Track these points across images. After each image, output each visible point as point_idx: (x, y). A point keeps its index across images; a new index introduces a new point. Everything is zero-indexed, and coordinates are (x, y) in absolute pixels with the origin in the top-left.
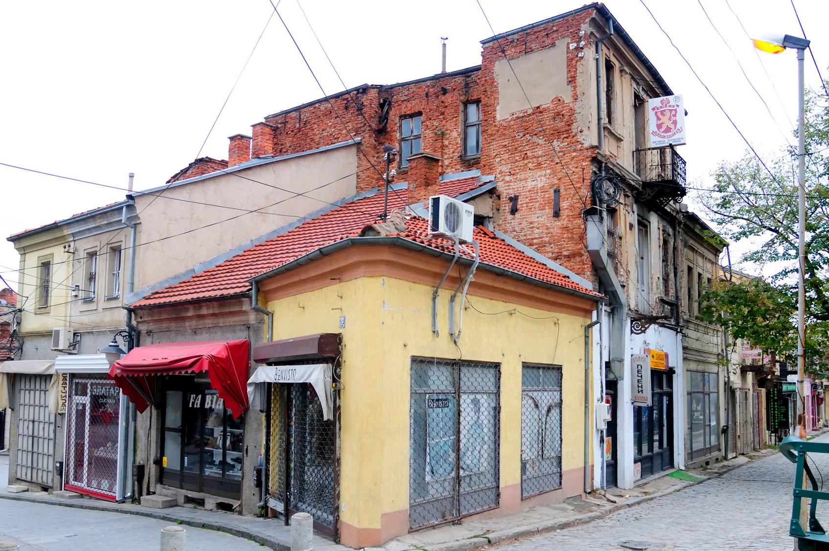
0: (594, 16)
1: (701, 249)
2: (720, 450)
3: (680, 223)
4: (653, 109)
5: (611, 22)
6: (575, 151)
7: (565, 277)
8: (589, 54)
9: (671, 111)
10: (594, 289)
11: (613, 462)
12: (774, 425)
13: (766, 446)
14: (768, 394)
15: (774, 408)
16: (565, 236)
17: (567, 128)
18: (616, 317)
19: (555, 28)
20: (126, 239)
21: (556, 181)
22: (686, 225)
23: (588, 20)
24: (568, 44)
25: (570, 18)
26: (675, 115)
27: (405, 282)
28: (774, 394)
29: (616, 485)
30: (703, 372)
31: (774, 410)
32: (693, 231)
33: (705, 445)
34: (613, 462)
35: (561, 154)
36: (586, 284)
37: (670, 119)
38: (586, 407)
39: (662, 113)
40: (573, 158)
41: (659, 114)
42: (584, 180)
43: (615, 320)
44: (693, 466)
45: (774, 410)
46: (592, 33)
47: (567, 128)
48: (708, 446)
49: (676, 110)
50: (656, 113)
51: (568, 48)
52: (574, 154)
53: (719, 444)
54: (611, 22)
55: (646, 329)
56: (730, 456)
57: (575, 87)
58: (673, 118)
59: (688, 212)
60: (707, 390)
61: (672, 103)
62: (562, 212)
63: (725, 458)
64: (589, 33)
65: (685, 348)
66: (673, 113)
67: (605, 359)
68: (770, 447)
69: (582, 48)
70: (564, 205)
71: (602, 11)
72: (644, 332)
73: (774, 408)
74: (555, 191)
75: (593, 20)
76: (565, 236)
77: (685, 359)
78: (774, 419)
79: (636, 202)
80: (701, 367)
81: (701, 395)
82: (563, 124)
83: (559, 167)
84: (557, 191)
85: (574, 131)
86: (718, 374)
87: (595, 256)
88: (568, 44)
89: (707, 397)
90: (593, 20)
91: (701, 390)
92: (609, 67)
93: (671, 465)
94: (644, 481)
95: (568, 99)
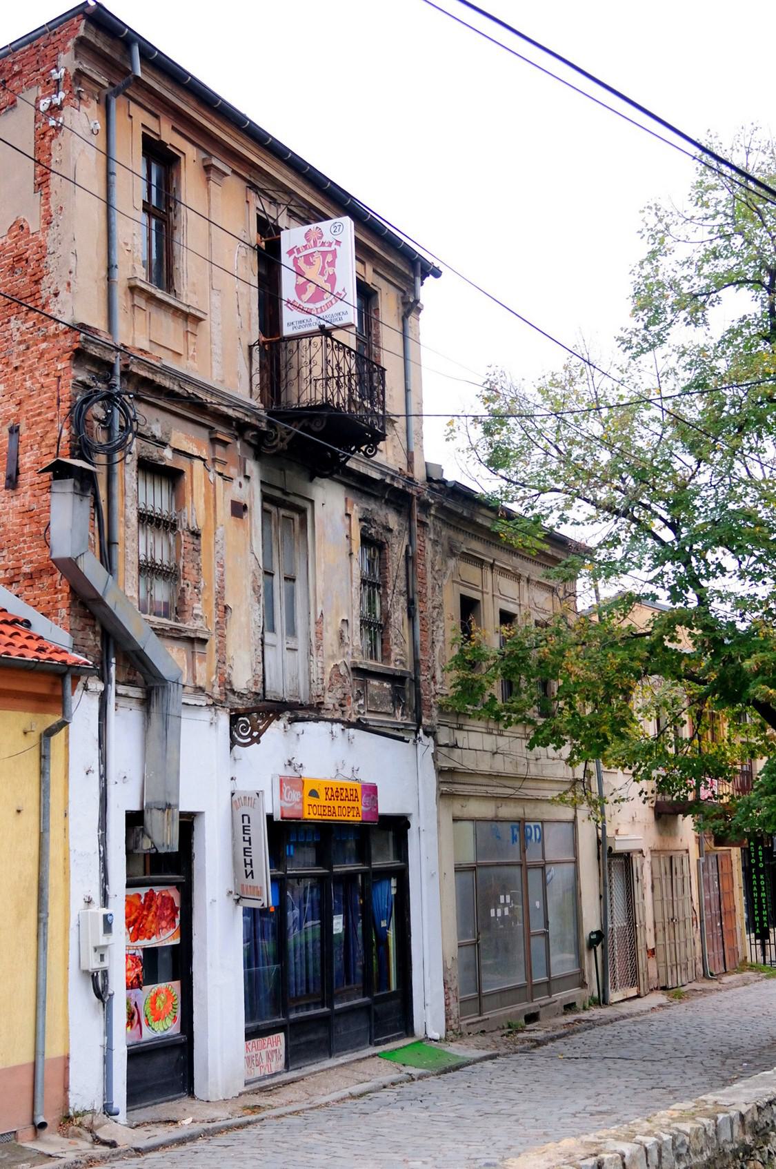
0: (81, 32)
1: (505, 560)
2: (583, 985)
3: (425, 506)
4: (290, 252)
5: (136, 50)
6: (45, 338)
7: (15, 621)
8: (83, 119)
9: (324, 254)
10: (76, 648)
11: (183, 1038)
12: (761, 922)
13: (744, 966)
14: (746, 854)
15: (759, 886)
16: (27, 529)
17: (34, 289)
18: (154, 710)
19: (16, 68)
20: (283, 772)
21: (13, 409)
22: (441, 508)
23: (70, 44)
24: (37, 101)
25: (41, 42)
26: (332, 264)
27: (22, 713)
28: (757, 857)
29: (191, 1093)
30: (521, 823)
31: (759, 891)
32: (471, 522)
33: (529, 974)
34: (183, 1038)
35: (23, 347)
36: (56, 635)
37: (322, 273)
38: (39, 920)
39: (308, 260)
40: (42, 354)
41: (301, 263)
42: (59, 401)
43: (154, 716)
44: (479, 1027)
45: (759, 891)
46: (79, 73)
47: (34, 289)
48: (539, 978)
49: (334, 253)
50: (295, 260)
51: (37, 109)
52: (44, 345)
53: (582, 971)
54: (136, 50)
55: (261, 733)
56: (614, 996)
57: (47, 196)
58: (329, 270)
59: (444, 482)
60: (533, 856)
61: (327, 237)
62: (22, 477)
63: (602, 1001)
64: (72, 72)
65: (440, 772)
66: (329, 258)
67: (124, 800)
68: (752, 968)
69: (60, 108)
70: (27, 460)
71: (101, 20)
72: (256, 740)
73: (759, 886)
74: (11, 431)
75: (82, 43)
76: (27, 529)
77: (442, 795)
78: (760, 909)
79: (258, 456)
80: (509, 811)
81: (516, 871)
82: (26, 279)
83: (18, 376)
84: (14, 431)
85: (44, 294)
86: (574, 822)
87: (69, 567)
88: (37, 101)
89: (534, 876)
90: (82, 43)
91: (517, 859)
92: (155, 151)
93: (405, 1024)
94: (293, 1074)
95: (34, 225)
